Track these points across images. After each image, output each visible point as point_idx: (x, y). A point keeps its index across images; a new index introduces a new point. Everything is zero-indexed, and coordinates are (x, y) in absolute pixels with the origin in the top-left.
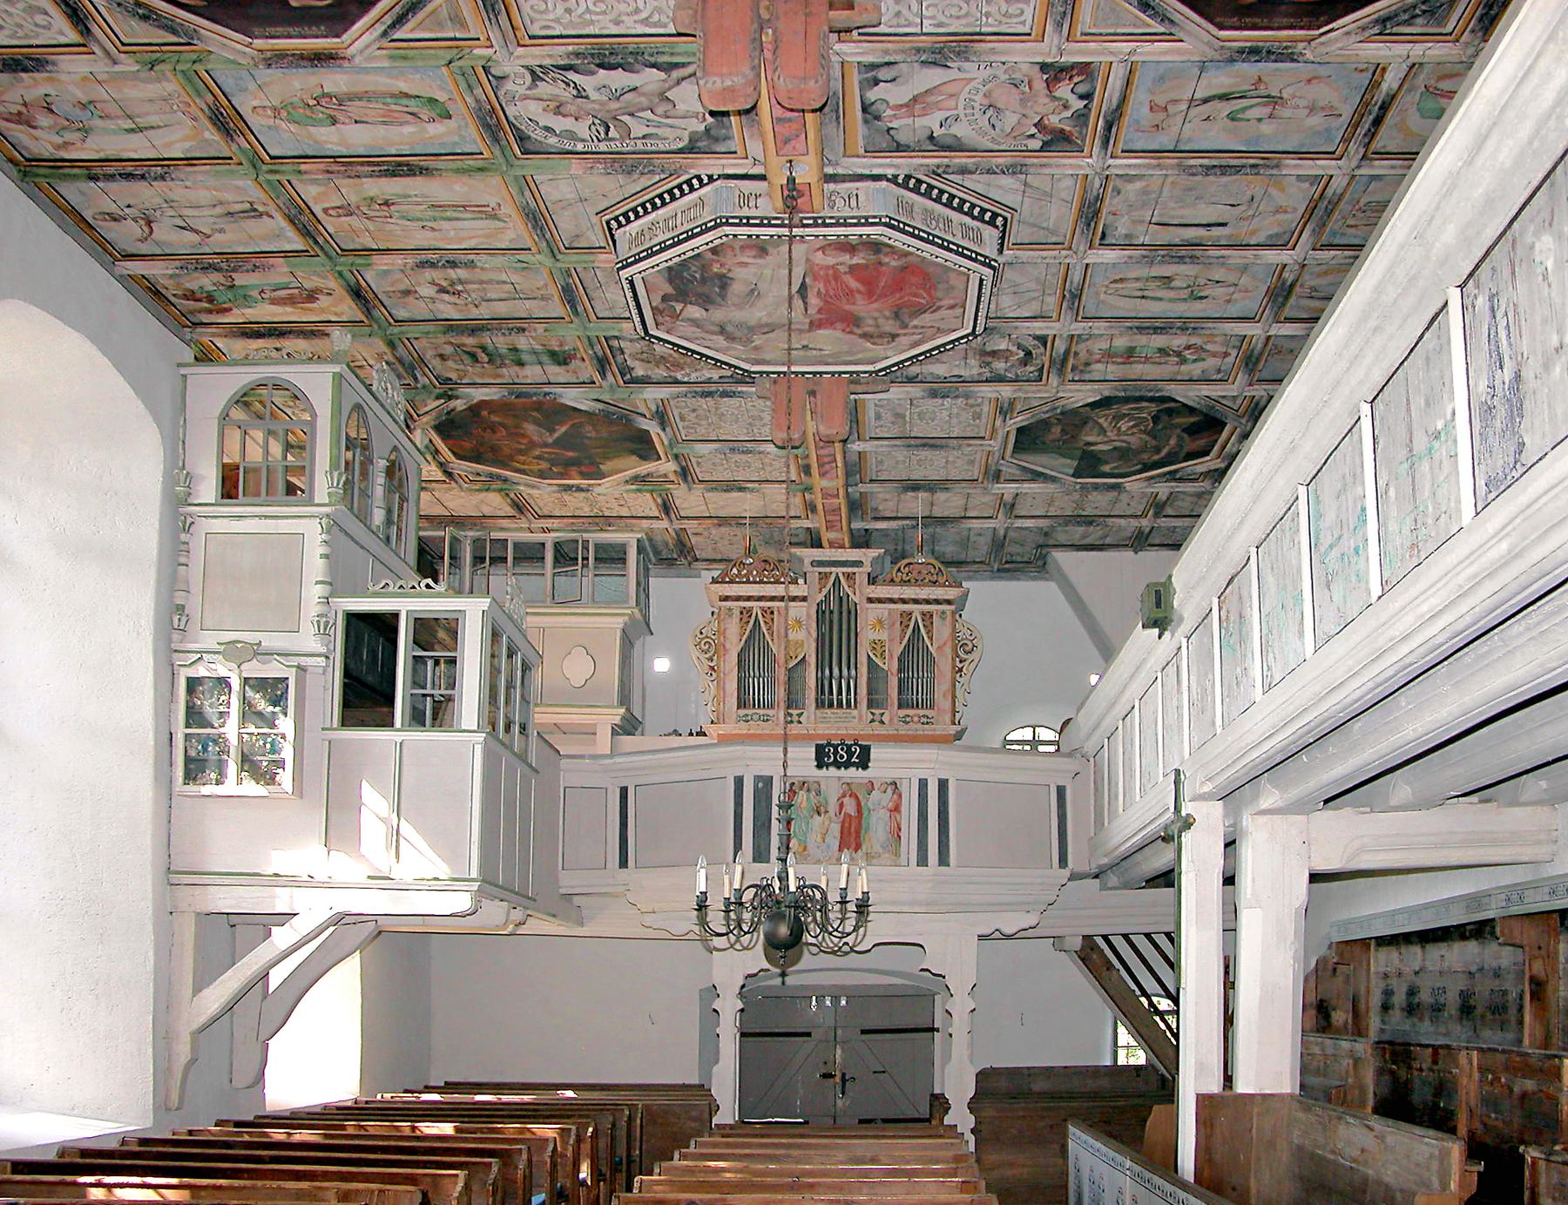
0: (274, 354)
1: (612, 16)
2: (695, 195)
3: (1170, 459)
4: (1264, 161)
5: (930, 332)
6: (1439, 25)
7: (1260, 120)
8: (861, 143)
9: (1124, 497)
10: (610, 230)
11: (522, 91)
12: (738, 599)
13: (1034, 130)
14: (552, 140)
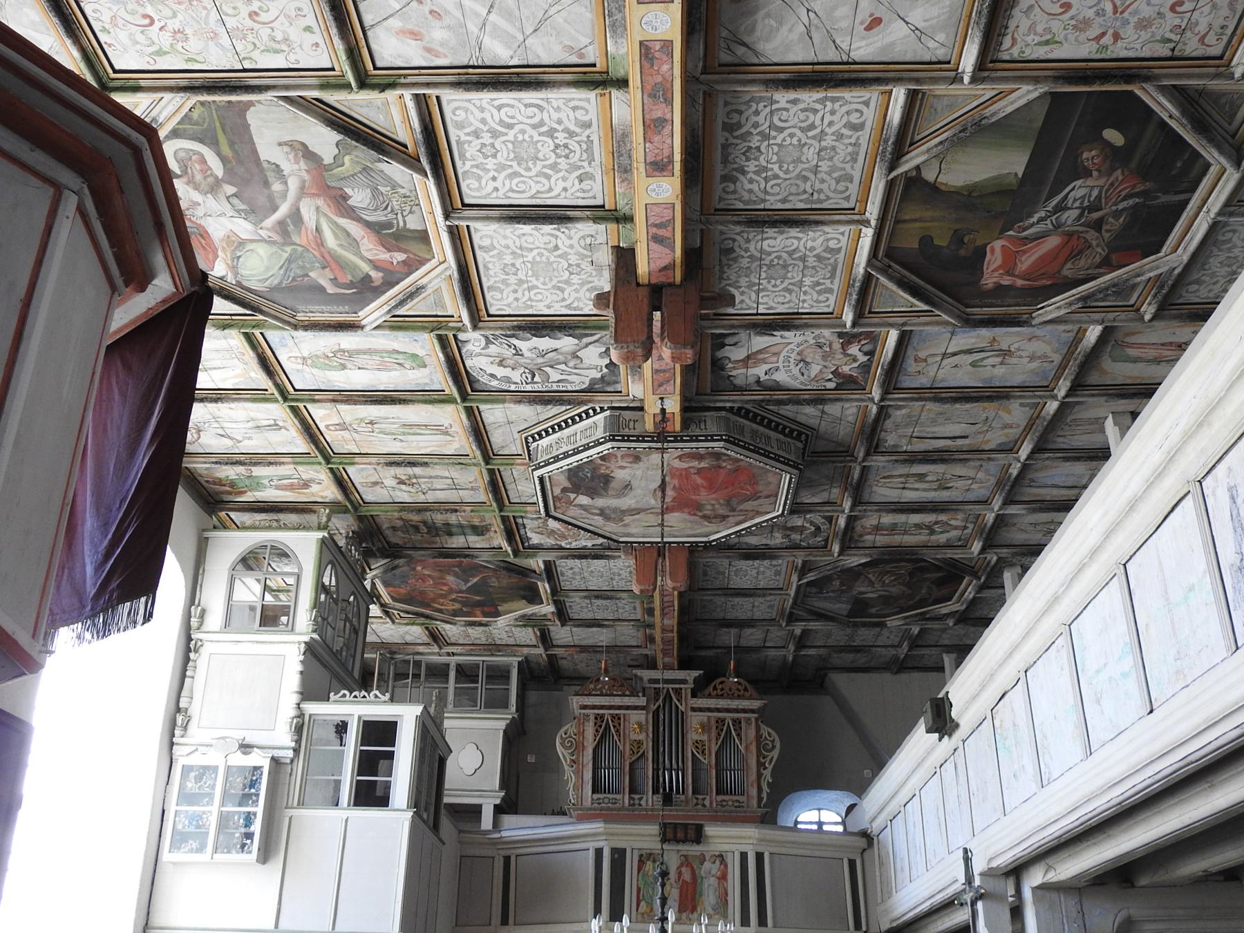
0: (275, 524)
1: (546, 303)
2: (590, 420)
3: (922, 603)
4: (996, 394)
5: (751, 514)
6: (1124, 300)
7: (993, 366)
8: (709, 385)
9: (885, 632)
10: (527, 443)
11: (478, 350)
12: (594, 707)
13: (831, 376)
14: (494, 383)
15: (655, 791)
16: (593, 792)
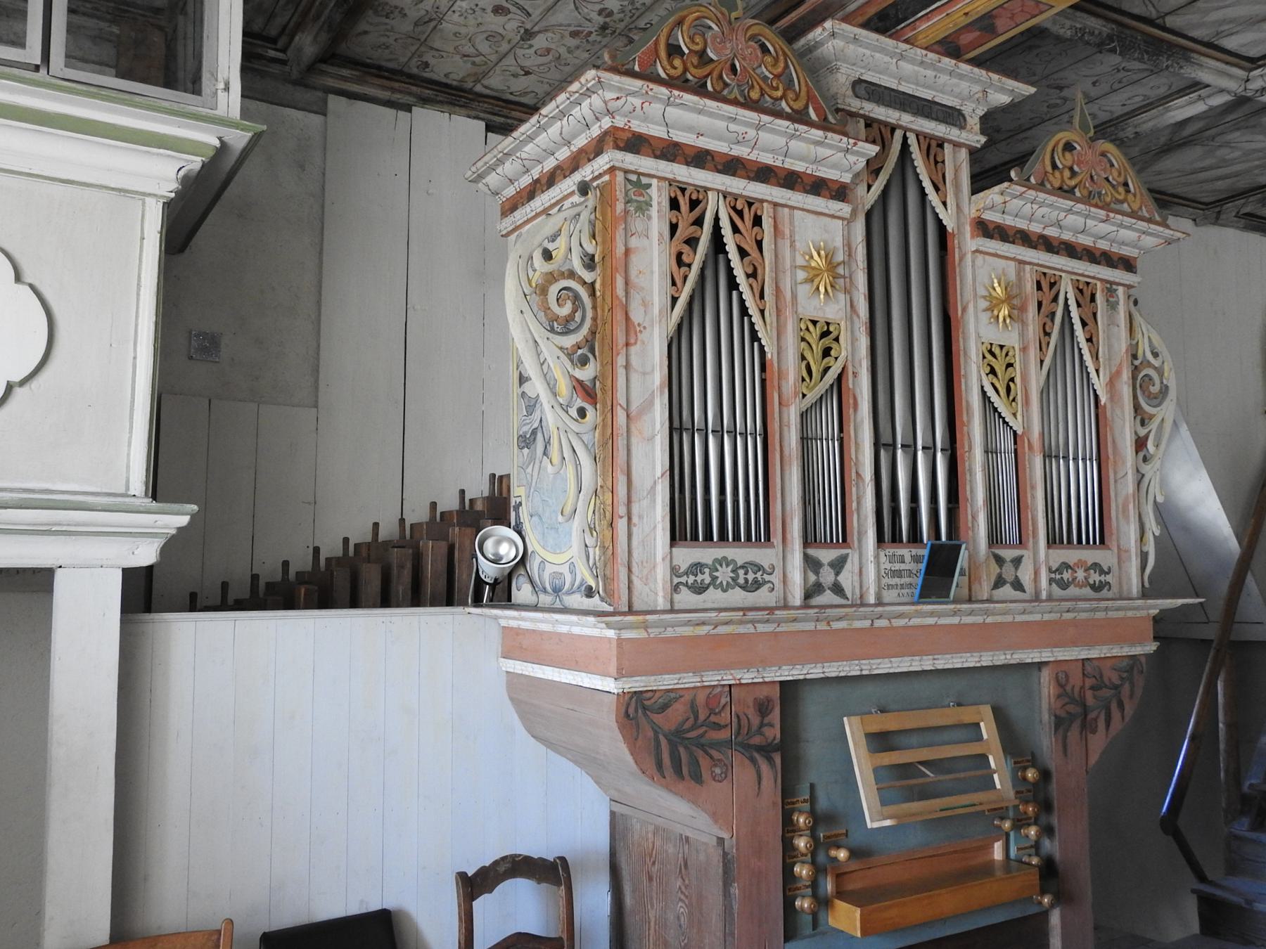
12: (670, 151)
15: (888, 534)
16: (677, 536)
